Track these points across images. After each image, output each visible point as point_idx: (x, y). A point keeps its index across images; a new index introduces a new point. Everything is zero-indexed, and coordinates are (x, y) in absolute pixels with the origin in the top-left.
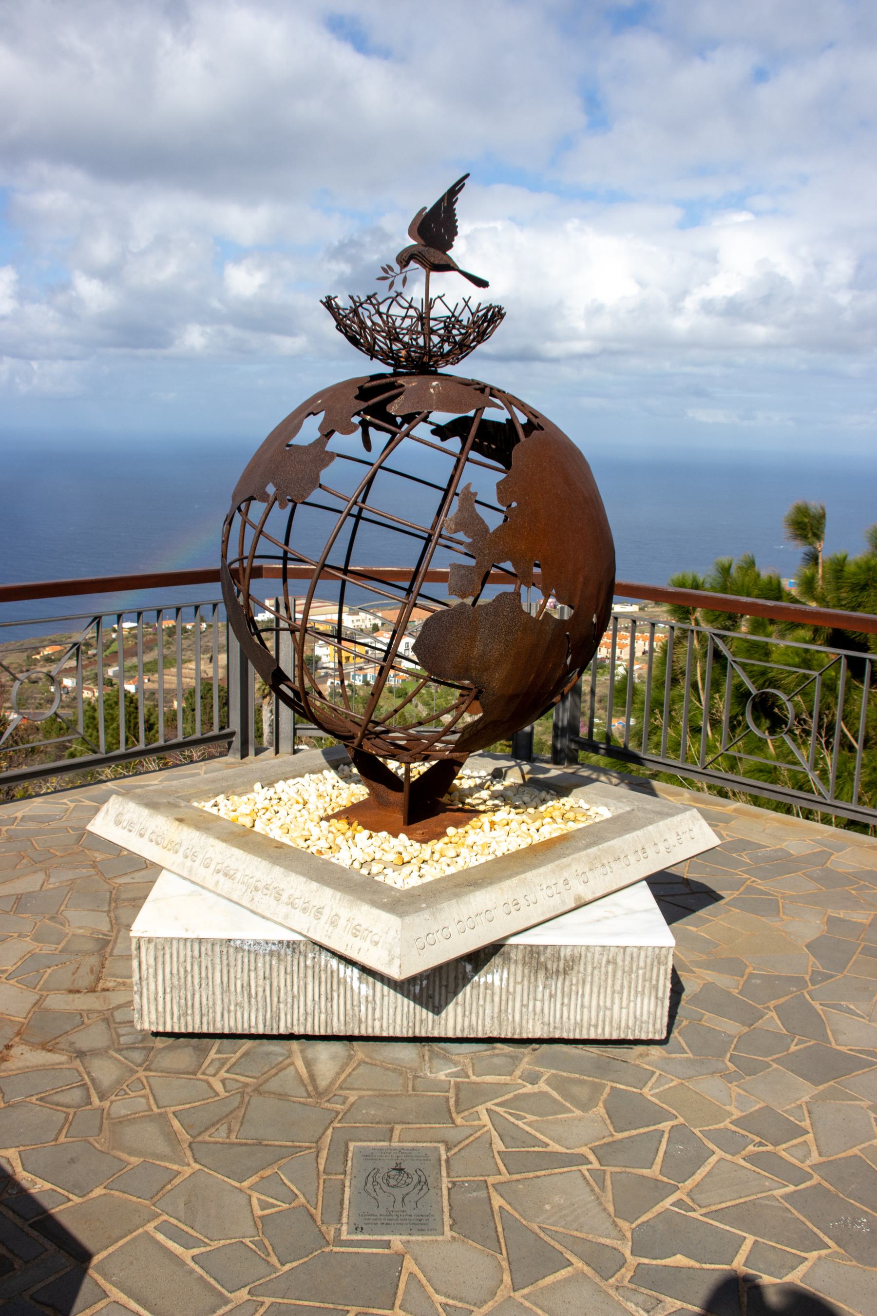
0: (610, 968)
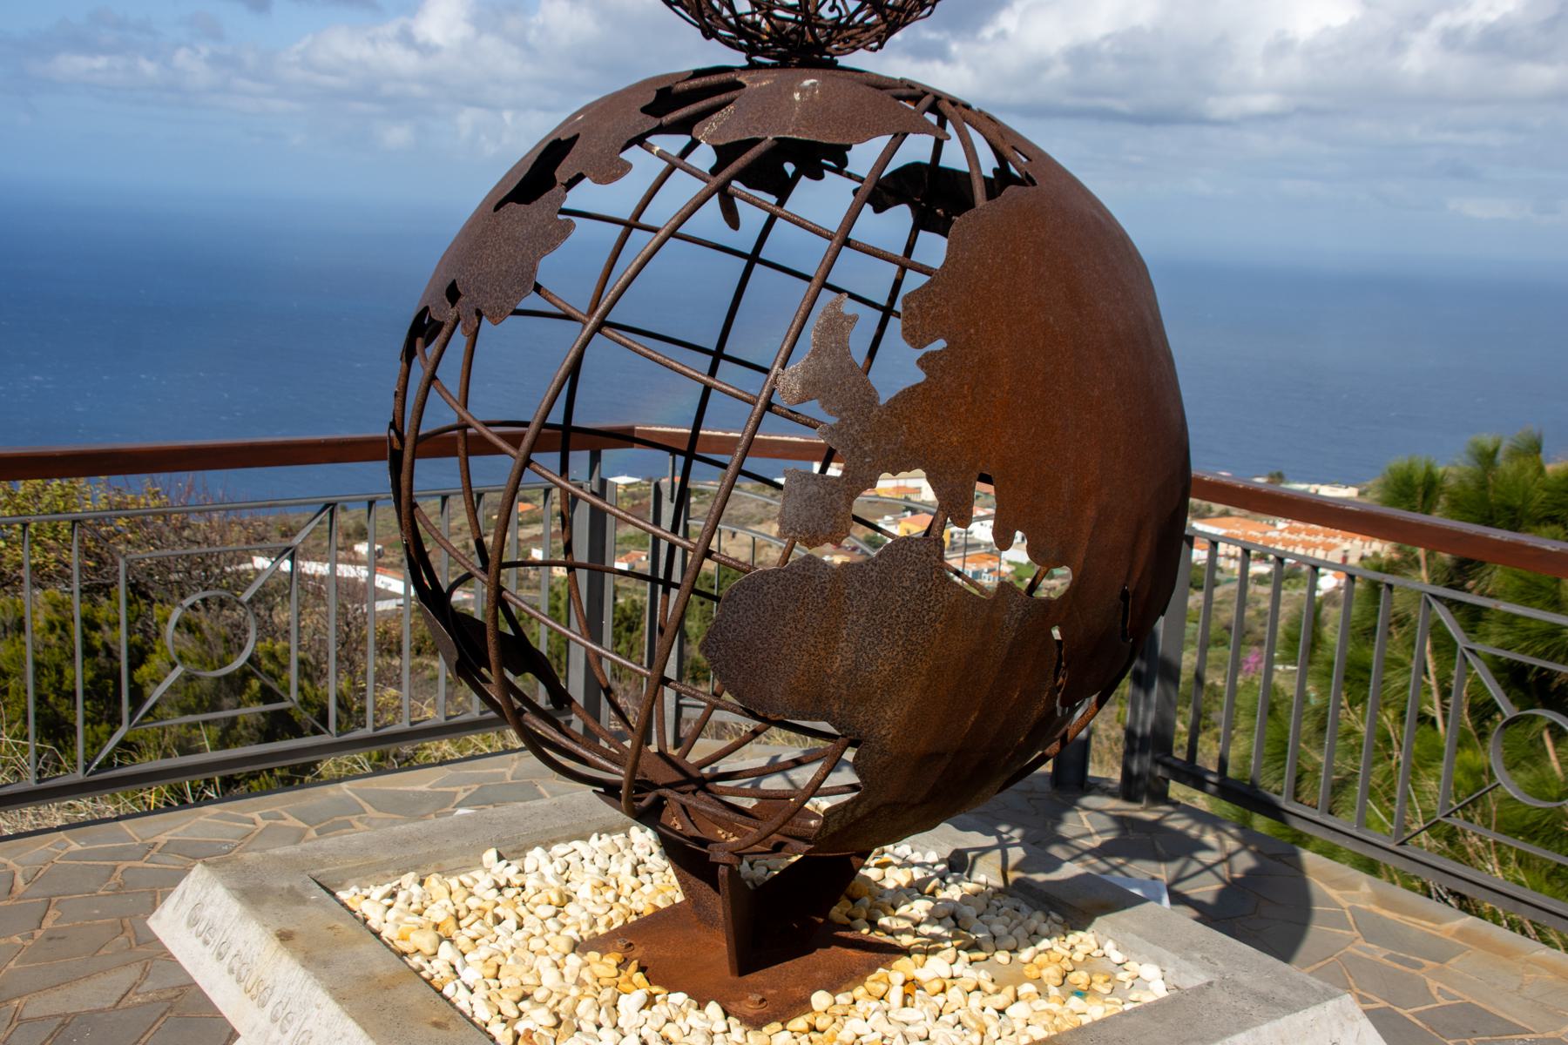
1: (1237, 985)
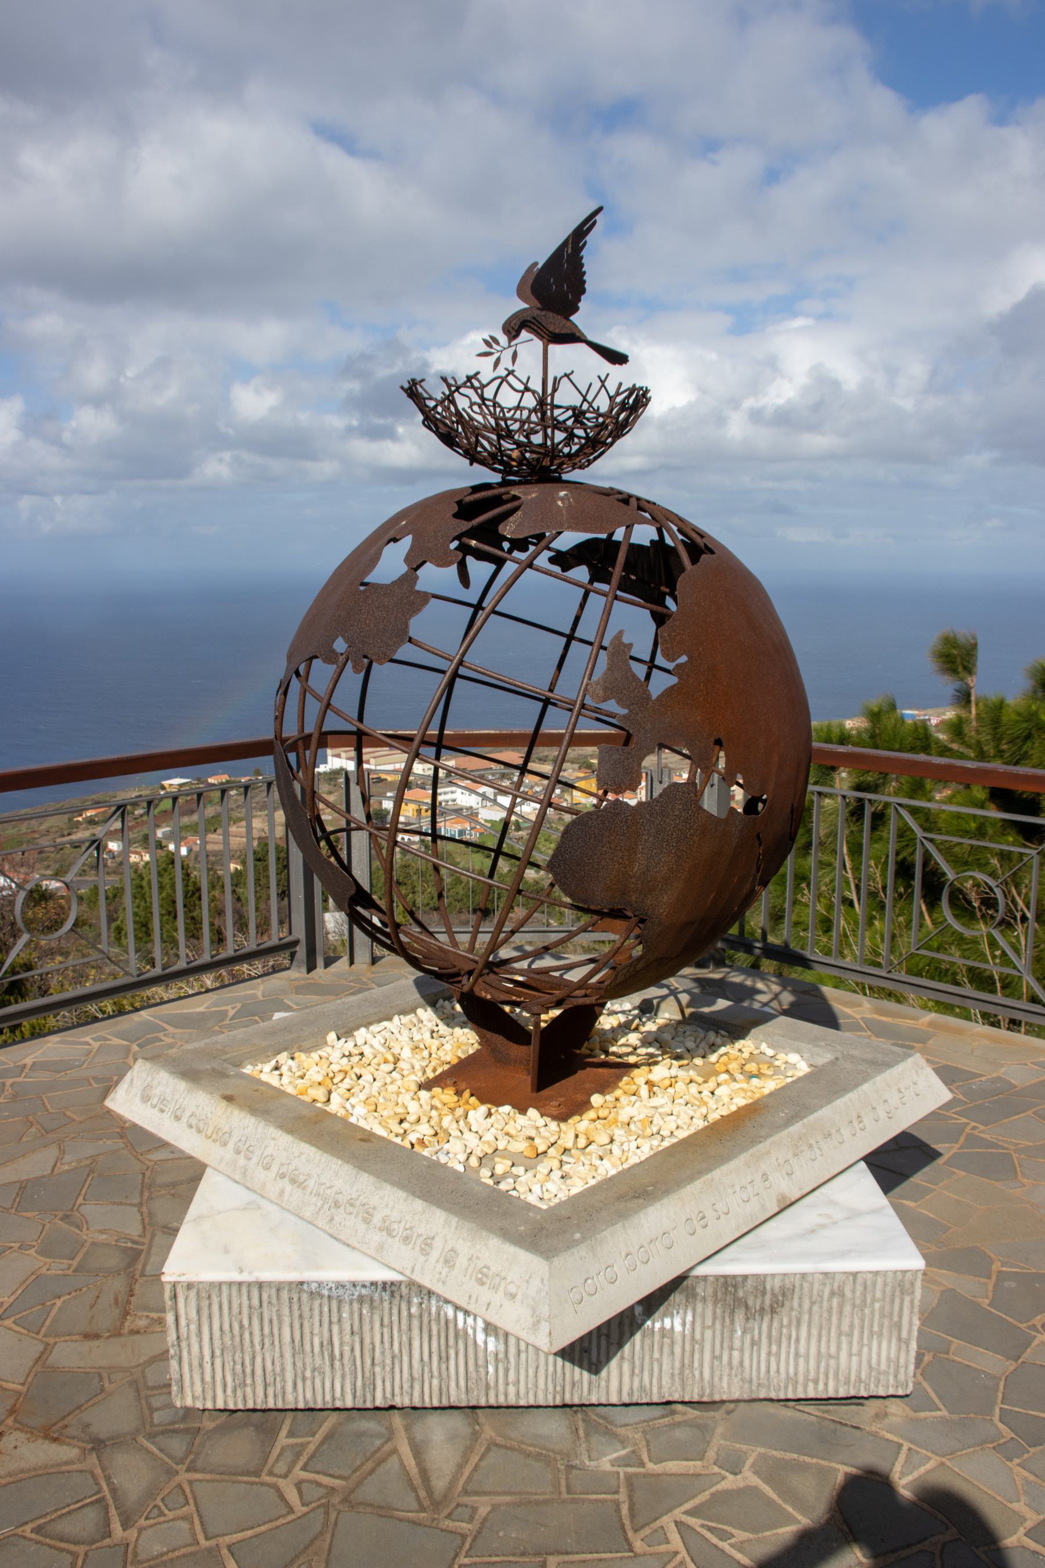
0: (835, 1302)
1: (853, 1057)
